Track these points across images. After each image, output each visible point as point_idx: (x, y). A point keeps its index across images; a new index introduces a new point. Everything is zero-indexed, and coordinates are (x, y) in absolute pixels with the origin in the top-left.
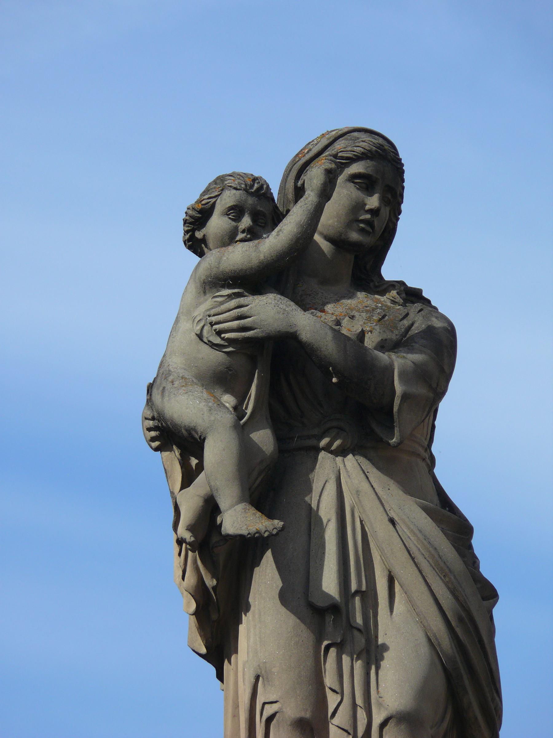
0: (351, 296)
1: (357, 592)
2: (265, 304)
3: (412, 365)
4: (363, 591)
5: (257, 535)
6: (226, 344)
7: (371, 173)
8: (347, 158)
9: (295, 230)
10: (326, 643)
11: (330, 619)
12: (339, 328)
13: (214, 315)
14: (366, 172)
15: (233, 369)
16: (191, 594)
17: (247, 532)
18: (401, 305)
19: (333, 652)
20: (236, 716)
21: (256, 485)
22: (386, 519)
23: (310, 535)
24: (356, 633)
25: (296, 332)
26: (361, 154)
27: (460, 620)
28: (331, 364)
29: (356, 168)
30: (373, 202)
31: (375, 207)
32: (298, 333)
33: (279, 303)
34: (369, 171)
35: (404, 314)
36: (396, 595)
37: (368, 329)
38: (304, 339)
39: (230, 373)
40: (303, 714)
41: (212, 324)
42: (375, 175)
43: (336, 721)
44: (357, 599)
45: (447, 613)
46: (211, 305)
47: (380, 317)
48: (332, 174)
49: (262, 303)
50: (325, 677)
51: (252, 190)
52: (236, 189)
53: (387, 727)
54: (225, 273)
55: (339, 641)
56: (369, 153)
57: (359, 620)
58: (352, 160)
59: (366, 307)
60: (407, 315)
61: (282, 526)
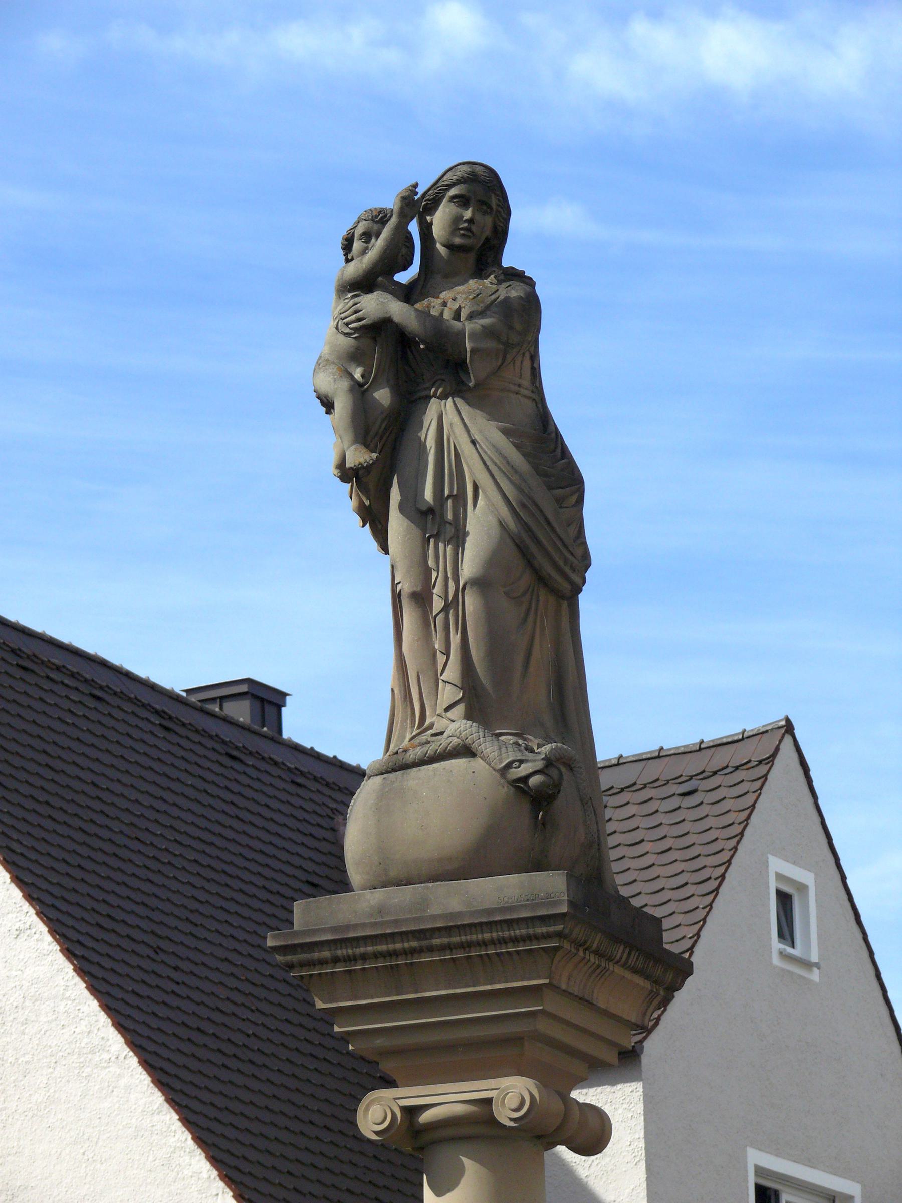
0: (465, 281)
1: (449, 496)
3: (480, 327)
5: (360, 466)
8: (447, 185)
10: (427, 535)
19: (432, 541)
22: (468, 440)
24: (448, 526)
25: (390, 316)
27: (523, 506)
29: (453, 192)
30: (468, 214)
34: (463, 193)
35: (493, 291)
36: (480, 494)
37: (463, 306)
40: (415, 589)
41: (343, 319)
43: (435, 591)
44: (450, 502)
52: (365, 220)
53: (466, 591)
57: (450, 516)
58: (450, 187)
60: (498, 290)
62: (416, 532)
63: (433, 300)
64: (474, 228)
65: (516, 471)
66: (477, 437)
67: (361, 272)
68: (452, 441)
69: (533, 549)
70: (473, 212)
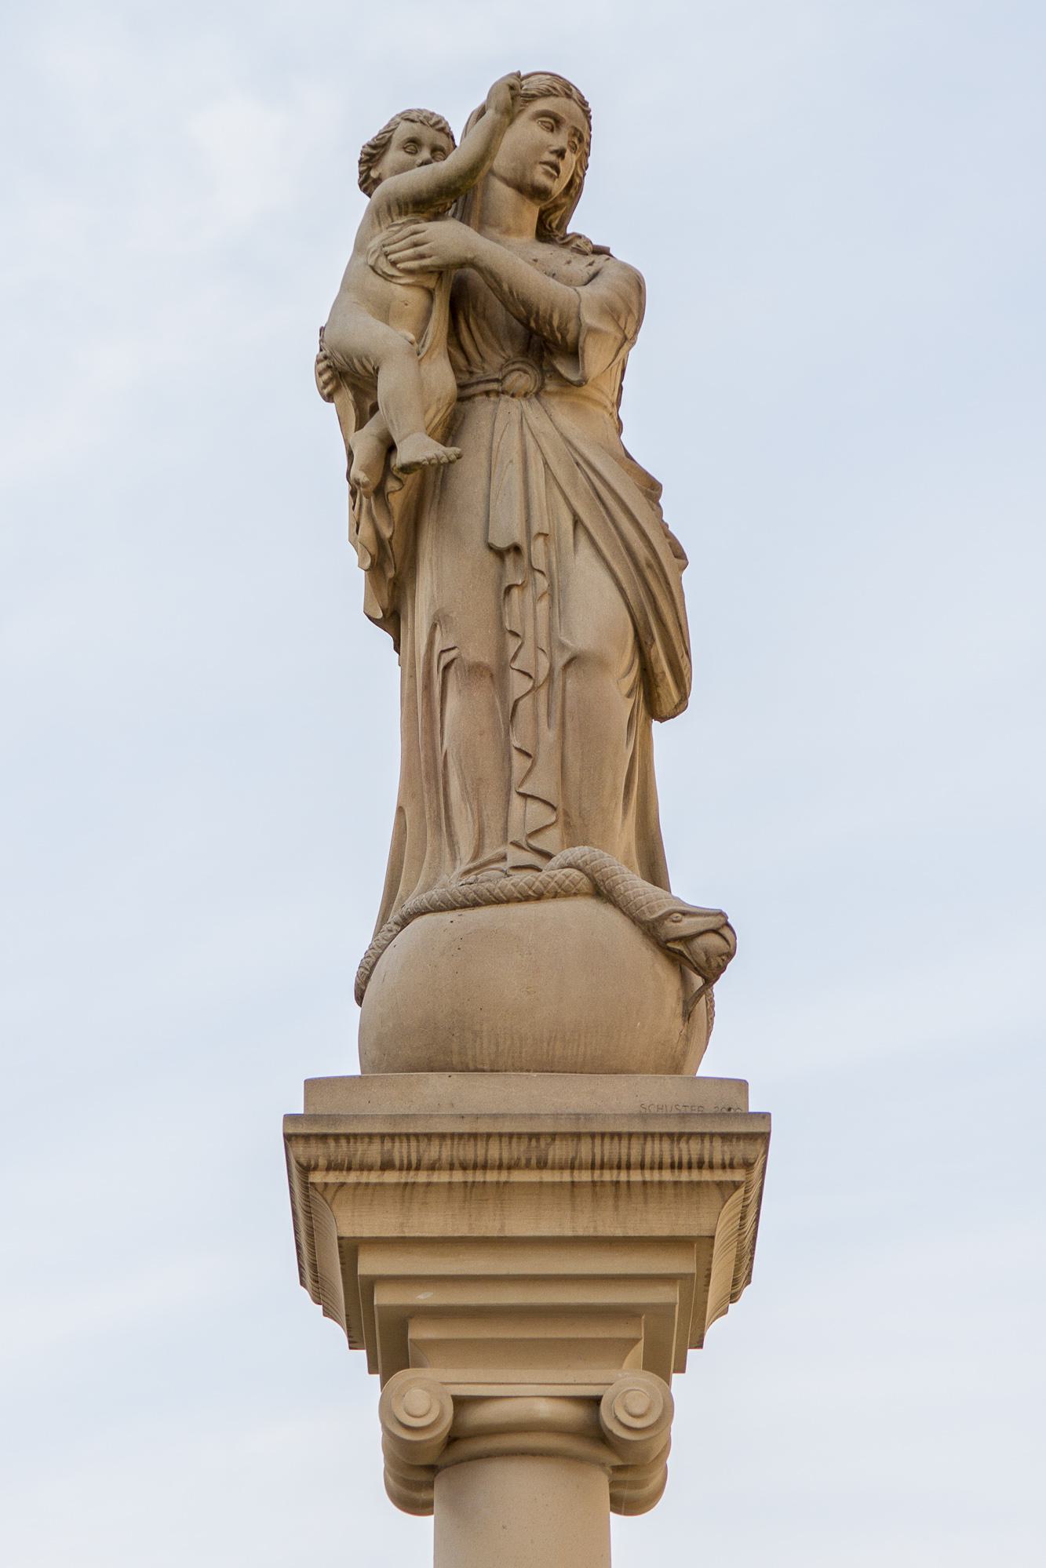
11: (509, 560)
20: (413, 676)
21: (433, 425)
23: (490, 478)
24: (538, 575)
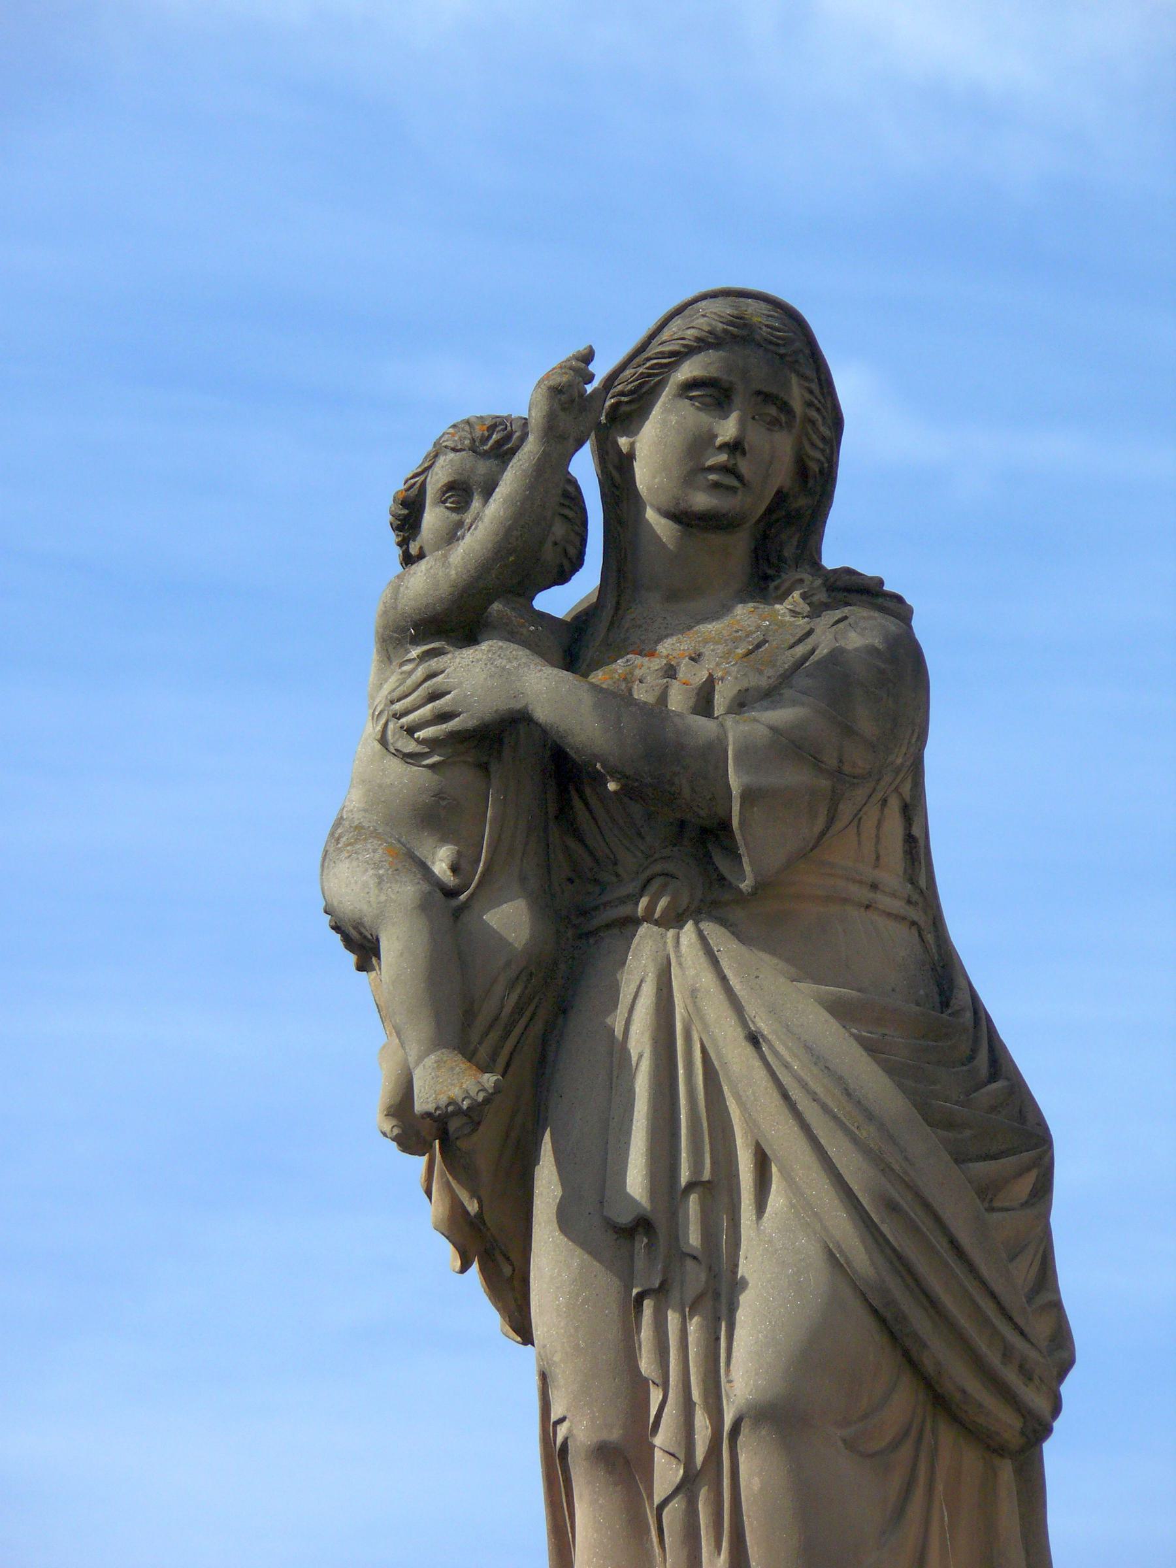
0: (724, 609)
1: (691, 1186)
2: (470, 663)
3: (766, 731)
4: (708, 1182)
5: (450, 1108)
6: (427, 750)
7: (715, 375)
8: (672, 354)
9: (502, 513)
10: (635, 1291)
12: (667, 682)
13: (399, 700)
14: (706, 374)
15: (449, 796)
16: (443, 1234)
17: (434, 1106)
18: (807, 617)
19: (648, 1305)
24: (689, 1263)
25: (526, 707)
26: (695, 342)
28: (597, 757)
29: (686, 371)
30: (728, 429)
31: (731, 438)
32: (530, 708)
33: (496, 656)
34: (713, 372)
36: (774, 1182)
38: (542, 717)
39: (444, 803)
41: (398, 716)
42: (725, 377)
43: (658, 1440)
44: (693, 1199)
45: (859, 1195)
46: (396, 681)
47: (750, 648)
48: (564, 393)
49: (466, 662)
50: (641, 1357)
51: (485, 448)
52: (455, 450)
54: (406, 617)
55: (657, 1286)
56: (710, 336)
57: (694, 1238)
58: (679, 357)
59: (737, 631)
60: (810, 633)
61: (495, 1084)
62: (606, 1282)
63: (639, 660)
64: (744, 466)
65: (870, 1116)
66: (763, 1025)
67: (444, 589)
68: (695, 1037)
69: (920, 1322)
70: (742, 423)
